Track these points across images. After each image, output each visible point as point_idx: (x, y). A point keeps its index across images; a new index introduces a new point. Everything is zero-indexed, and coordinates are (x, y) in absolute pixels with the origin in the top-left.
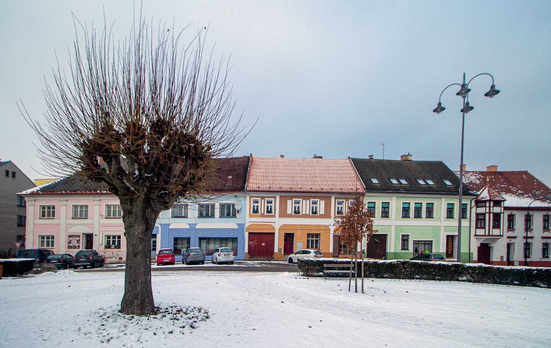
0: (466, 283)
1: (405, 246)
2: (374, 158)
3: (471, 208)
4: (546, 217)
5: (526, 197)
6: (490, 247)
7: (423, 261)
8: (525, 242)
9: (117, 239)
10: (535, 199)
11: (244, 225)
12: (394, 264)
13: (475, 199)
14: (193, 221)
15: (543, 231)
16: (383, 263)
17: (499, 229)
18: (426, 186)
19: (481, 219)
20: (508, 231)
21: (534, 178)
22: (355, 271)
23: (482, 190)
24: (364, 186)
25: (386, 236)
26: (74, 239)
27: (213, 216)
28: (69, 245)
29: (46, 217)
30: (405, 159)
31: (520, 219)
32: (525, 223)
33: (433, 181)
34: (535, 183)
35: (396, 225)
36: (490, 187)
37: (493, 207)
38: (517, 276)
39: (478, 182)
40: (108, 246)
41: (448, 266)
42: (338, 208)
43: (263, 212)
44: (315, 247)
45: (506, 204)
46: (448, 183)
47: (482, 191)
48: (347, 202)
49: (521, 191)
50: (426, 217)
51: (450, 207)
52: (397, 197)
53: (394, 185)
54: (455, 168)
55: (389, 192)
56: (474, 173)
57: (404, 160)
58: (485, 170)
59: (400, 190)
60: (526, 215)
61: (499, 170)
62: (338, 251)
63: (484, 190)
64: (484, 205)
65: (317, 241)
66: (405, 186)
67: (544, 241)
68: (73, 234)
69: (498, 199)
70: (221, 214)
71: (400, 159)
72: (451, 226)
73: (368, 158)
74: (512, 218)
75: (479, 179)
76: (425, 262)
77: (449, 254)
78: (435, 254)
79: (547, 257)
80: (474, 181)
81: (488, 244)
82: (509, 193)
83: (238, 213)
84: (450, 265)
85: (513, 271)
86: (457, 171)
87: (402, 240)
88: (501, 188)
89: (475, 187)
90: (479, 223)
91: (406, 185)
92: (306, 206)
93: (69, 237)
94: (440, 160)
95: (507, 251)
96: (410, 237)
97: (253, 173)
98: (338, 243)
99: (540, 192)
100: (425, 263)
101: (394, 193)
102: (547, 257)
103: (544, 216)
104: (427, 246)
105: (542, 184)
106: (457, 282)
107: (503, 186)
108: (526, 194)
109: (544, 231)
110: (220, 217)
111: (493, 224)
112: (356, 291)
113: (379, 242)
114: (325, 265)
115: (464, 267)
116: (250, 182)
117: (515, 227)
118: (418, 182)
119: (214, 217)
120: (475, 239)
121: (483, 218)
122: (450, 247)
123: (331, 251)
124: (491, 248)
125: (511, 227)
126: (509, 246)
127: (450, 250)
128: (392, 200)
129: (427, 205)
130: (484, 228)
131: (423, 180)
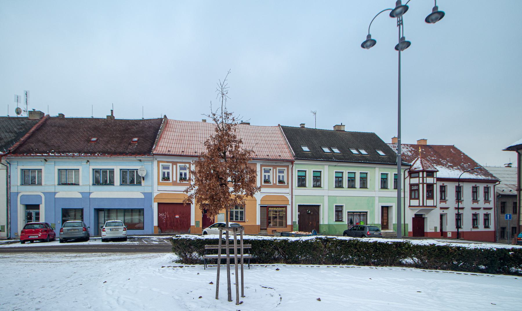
0: (413, 269)
1: (339, 218)
2: (306, 126)
3: (405, 179)
4: (475, 188)
5: (456, 169)
6: (424, 218)
7: (352, 238)
8: (457, 212)
10: (464, 171)
11: (151, 194)
12: (311, 243)
13: (408, 170)
14: (86, 190)
15: (472, 202)
16: (295, 241)
17: (433, 200)
18: (359, 155)
19: (415, 190)
20: (441, 202)
21: (461, 152)
23: (414, 161)
24: (294, 153)
25: (318, 206)
27: (112, 183)
30: (339, 130)
31: (451, 189)
32: (456, 194)
33: (366, 151)
34: (462, 157)
35: (329, 195)
36: (422, 158)
37: (426, 177)
38: (485, 259)
39: (409, 154)
41: (386, 244)
42: (265, 176)
43: (275, 182)
44: (236, 219)
45: (439, 175)
46: (381, 153)
47: (415, 162)
48: (275, 170)
49: (450, 163)
50: (360, 188)
51: (384, 177)
52: (329, 165)
53: (326, 153)
54: (387, 140)
55: (320, 160)
56: (406, 145)
57: (337, 130)
58: (416, 143)
59: (332, 159)
60: (456, 187)
61: (428, 143)
62: (266, 223)
63: (416, 160)
64: (418, 176)
65: (242, 213)
66: (337, 155)
67: (474, 212)
69: (431, 170)
70: (123, 181)
71: (332, 129)
72: (388, 196)
73: (299, 126)
74: (444, 189)
75: (410, 152)
76: (355, 238)
77: (385, 226)
78: (370, 225)
79: (477, 227)
80: (406, 153)
81: (422, 215)
82: (439, 165)
83: (144, 179)
84: (390, 243)
85: (480, 252)
86: (390, 144)
87: (336, 211)
88: (432, 160)
89: (407, 158)
90: (413, 193)
91: (339, 154)
94: (373, 132)
95: (440, 222)
96: (344, 208)
97: (165, 135)
98: (266, 215)
99: (467, 165)
100: (356, 240)
101: (325, 161)
102: (477, 227)
103: (473, 187)
104: (362, 218)
105: (469, 157)
106: (399, 268)
107: (433, 158)
108: (455, 166)
109: (473, 202)
110: (121, 185)
111: (426, 195)
112: (230, 299)
113: (312, 213)
114: (207, 247)
115: (409, 246)
116: (159, 145)
117: (447, 198)
118: (351, 151)
119: (114, 185)
120: (409, 210)
121: (417, 188)
122: (385, 218)
123: (258, 223)
124: (425, 220)
125: (443, 199)
126: (441, 216)
127: (385, 221)
128: (324, 169)
130: (418, 198)
131: (356, 150)
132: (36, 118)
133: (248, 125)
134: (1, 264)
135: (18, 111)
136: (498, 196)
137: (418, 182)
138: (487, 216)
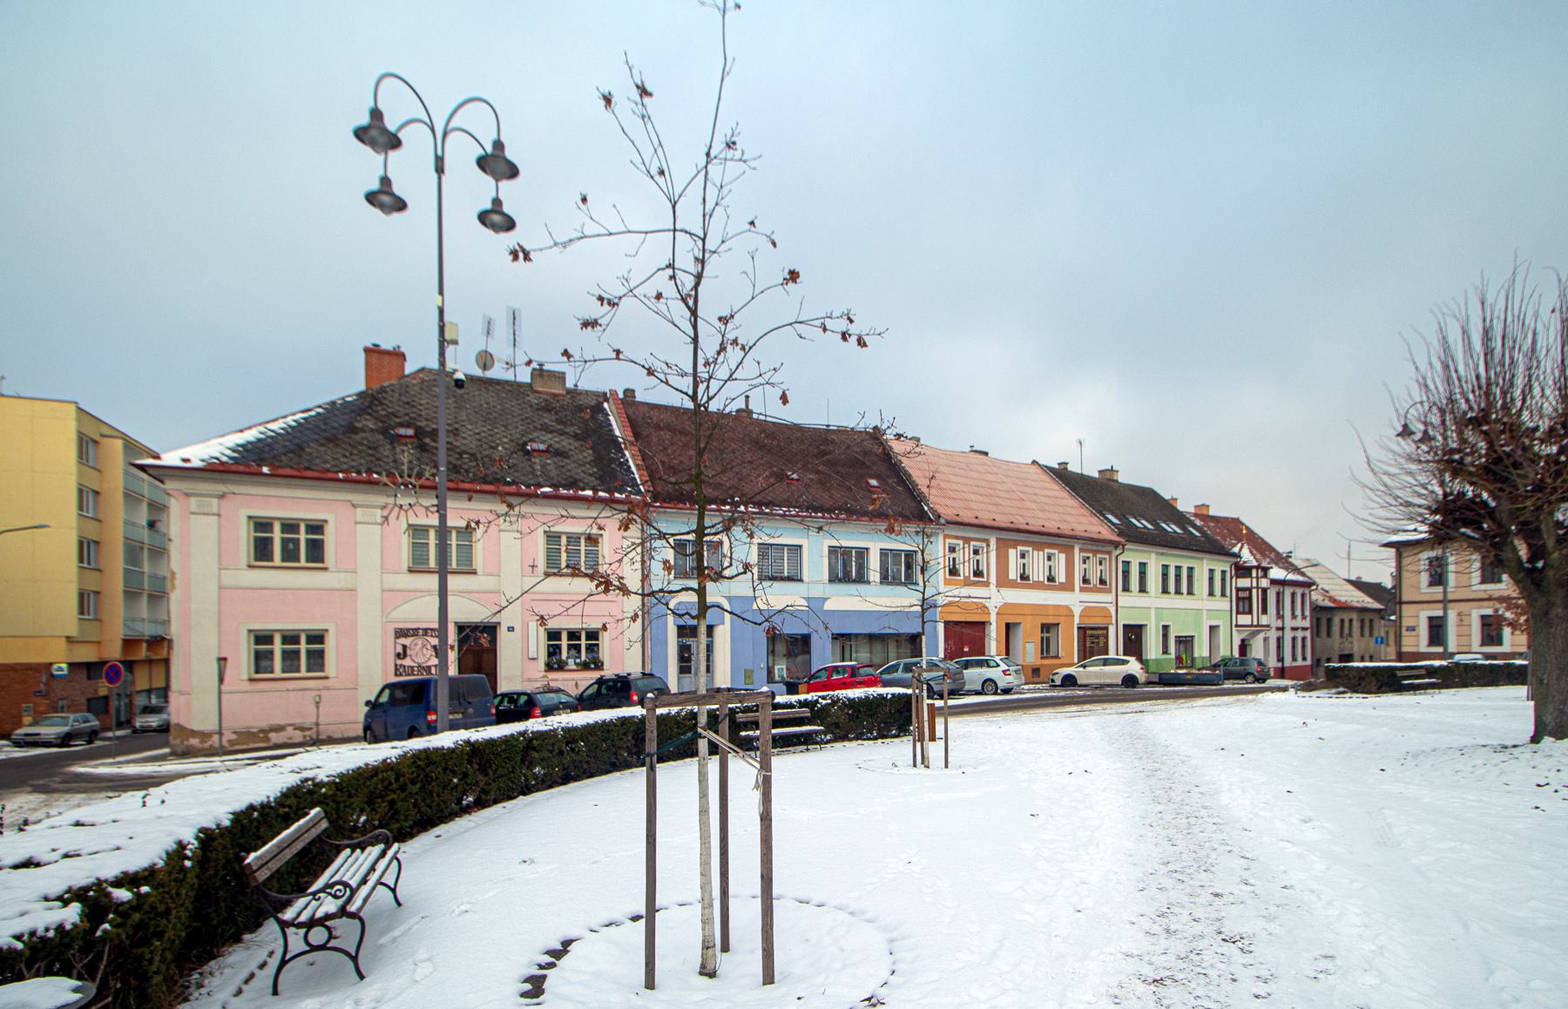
14: (817, 592)
19: (1244, 599)
22: (931, 706)
26: (420, 642)
28: (399, 662)
29: (303, 563)
40: (554, 663)
43: (967, 574)
61: (1212, 513)
68: (414, 626)
71: (1096, 475)
90: (1241, 604)
92: (1038, 564)
93: (397, 638)
130: (1250, 612)
132: (557, 392)
133: (983, 457)
134: (20, 803)
135: (486, 360)
137: (1405, 598)
138: (1304, 639)
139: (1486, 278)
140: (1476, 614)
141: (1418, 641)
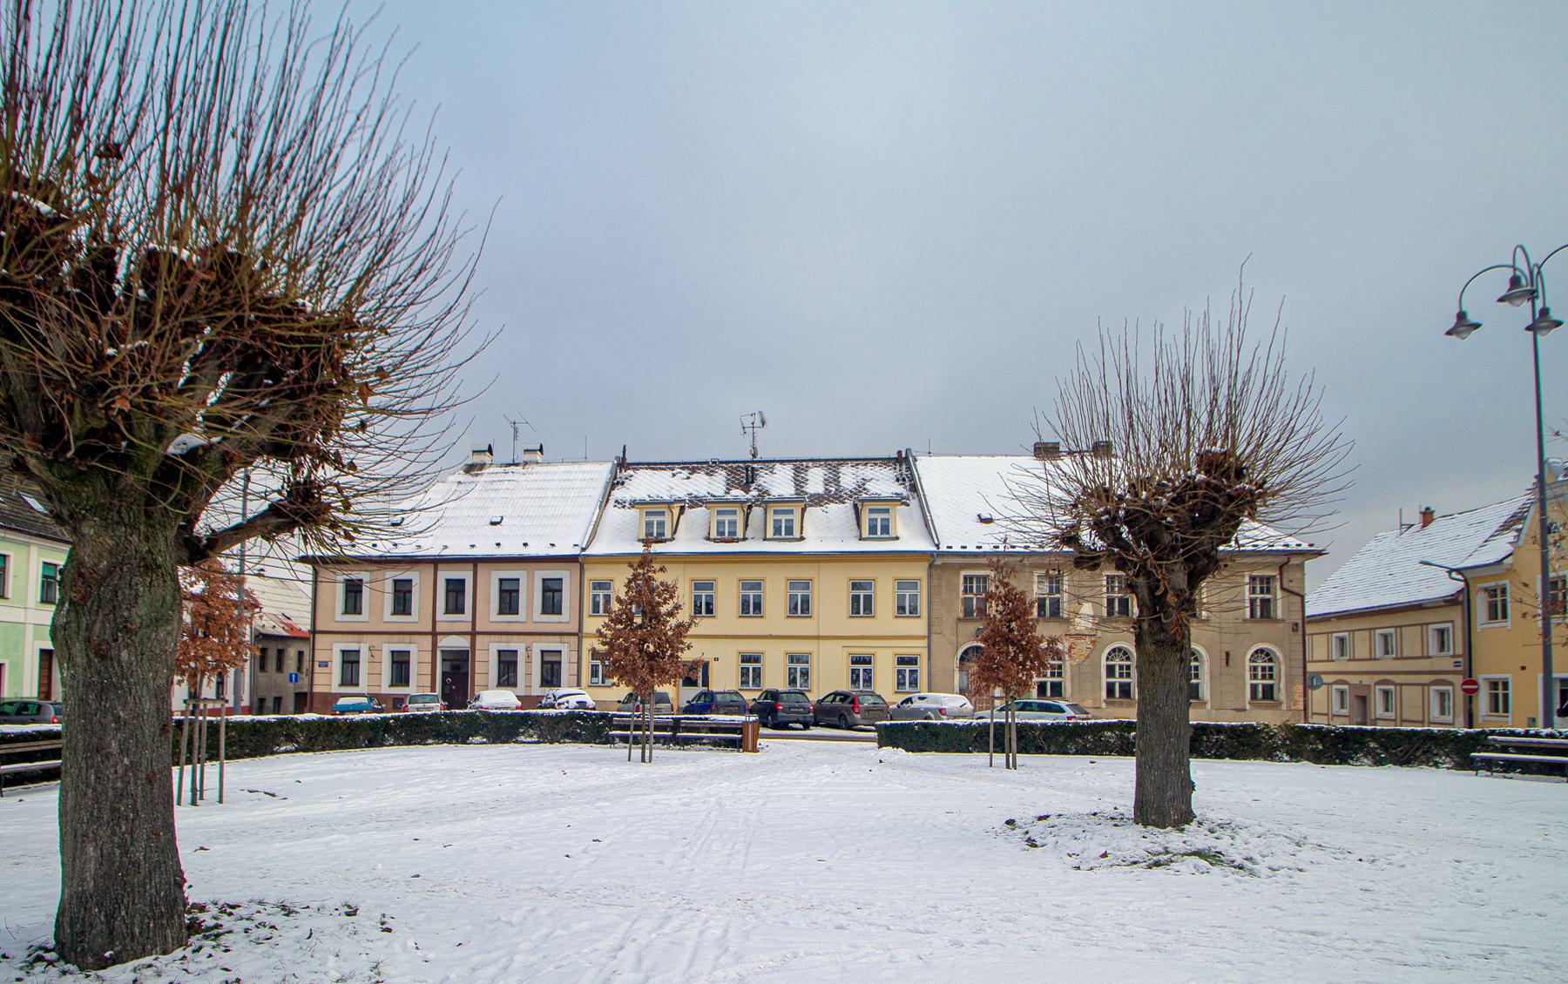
9: (1500, 692)
129: (44, 567)
136: (257, 637)
139: (307, 16)
140: (387, 647)
141: (331, 680)
